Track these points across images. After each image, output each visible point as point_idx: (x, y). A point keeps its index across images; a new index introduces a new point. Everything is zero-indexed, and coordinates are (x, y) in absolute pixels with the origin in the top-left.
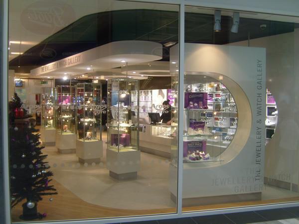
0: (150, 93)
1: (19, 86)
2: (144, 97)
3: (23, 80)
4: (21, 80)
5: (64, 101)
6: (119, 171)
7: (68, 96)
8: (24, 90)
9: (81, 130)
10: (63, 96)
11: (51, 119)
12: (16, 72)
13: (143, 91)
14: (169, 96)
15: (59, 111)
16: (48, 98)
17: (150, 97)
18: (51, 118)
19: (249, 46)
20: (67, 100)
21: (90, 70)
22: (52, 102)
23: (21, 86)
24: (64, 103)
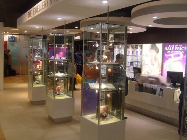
0: (139, 48)
1: (12, 41)
2: (131, 52)
3: (15, 36)
4: (14, 35)
5: (57, 55)
6: (54, 117)
7: (63, 47)
8: (16, 44)
9: (52, 83)
10: (56, 48)
11: (39, 75)
12: (5, 26)
13: (130, 45)
14: (166, 51)
15: (50, 66)
16: (36, 51)
17: (139, 52)
18: (39, 73)
19: (65, 20)
20: (61, 53)
21: (38, 28)
22: (41, 56)
23: (14, 41)
24: (57, 57)
